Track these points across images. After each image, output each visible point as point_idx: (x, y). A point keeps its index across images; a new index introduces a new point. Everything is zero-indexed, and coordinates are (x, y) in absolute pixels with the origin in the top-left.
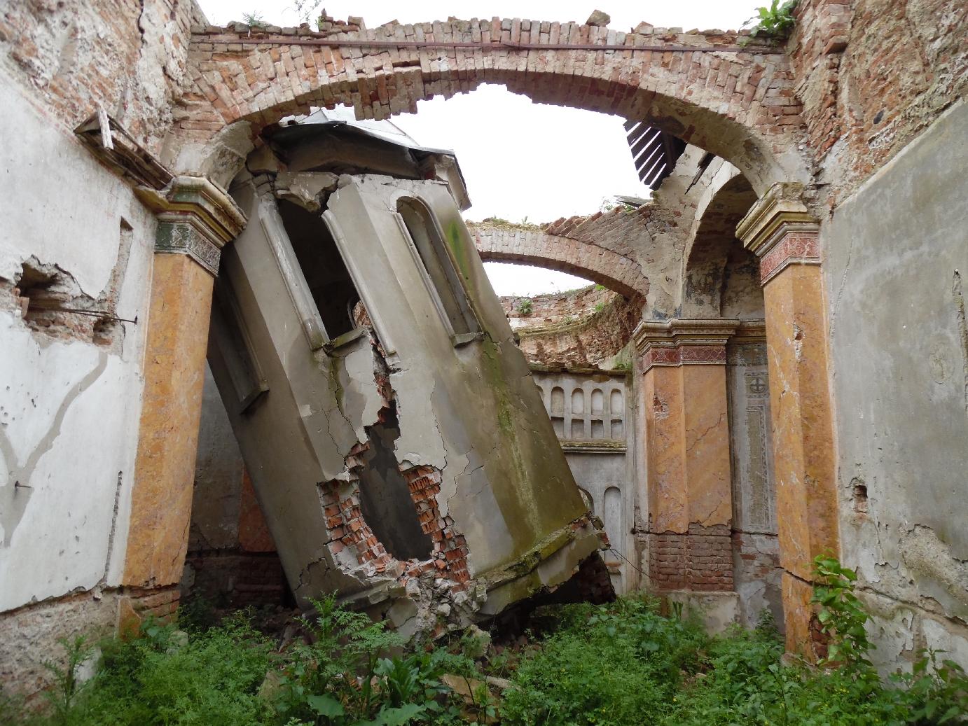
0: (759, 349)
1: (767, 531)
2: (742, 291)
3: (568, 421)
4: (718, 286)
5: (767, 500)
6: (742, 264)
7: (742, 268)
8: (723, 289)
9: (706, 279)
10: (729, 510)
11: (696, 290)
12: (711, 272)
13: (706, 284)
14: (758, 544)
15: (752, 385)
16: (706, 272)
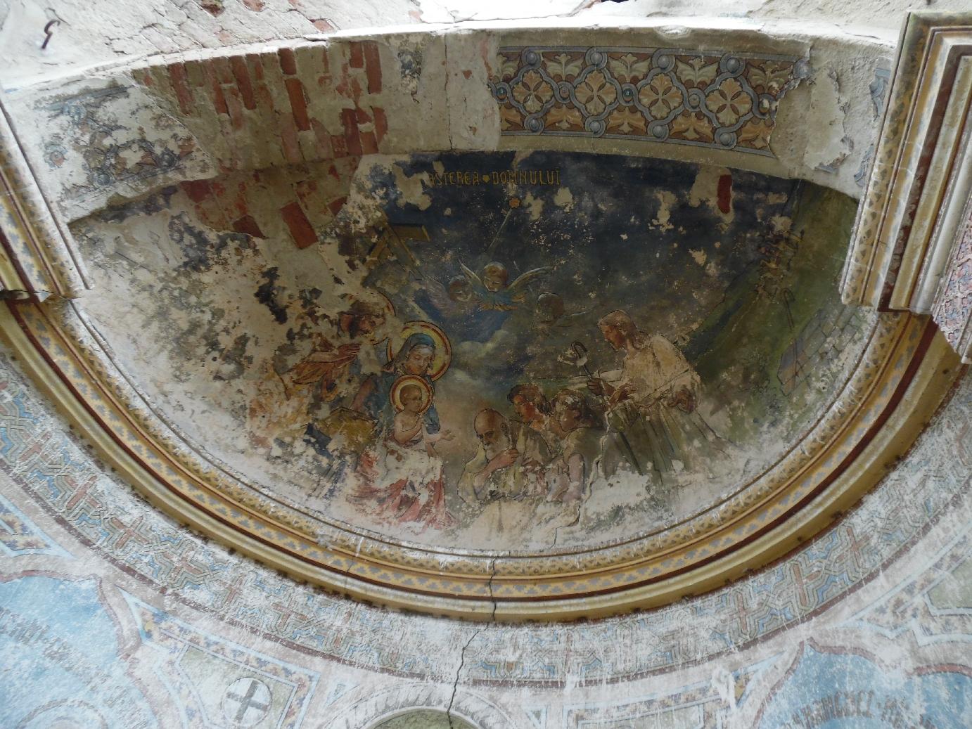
0: (16, 402)
2: (133, 264)
3: (604, 682)
4: (125, 190)
6: (199, 227)
7: (190, 230)
8: (117, 211)
9: (127, 146)
11: (81, 124)
12: (158, 150)
13: (115, 150)
16: (151, 136)
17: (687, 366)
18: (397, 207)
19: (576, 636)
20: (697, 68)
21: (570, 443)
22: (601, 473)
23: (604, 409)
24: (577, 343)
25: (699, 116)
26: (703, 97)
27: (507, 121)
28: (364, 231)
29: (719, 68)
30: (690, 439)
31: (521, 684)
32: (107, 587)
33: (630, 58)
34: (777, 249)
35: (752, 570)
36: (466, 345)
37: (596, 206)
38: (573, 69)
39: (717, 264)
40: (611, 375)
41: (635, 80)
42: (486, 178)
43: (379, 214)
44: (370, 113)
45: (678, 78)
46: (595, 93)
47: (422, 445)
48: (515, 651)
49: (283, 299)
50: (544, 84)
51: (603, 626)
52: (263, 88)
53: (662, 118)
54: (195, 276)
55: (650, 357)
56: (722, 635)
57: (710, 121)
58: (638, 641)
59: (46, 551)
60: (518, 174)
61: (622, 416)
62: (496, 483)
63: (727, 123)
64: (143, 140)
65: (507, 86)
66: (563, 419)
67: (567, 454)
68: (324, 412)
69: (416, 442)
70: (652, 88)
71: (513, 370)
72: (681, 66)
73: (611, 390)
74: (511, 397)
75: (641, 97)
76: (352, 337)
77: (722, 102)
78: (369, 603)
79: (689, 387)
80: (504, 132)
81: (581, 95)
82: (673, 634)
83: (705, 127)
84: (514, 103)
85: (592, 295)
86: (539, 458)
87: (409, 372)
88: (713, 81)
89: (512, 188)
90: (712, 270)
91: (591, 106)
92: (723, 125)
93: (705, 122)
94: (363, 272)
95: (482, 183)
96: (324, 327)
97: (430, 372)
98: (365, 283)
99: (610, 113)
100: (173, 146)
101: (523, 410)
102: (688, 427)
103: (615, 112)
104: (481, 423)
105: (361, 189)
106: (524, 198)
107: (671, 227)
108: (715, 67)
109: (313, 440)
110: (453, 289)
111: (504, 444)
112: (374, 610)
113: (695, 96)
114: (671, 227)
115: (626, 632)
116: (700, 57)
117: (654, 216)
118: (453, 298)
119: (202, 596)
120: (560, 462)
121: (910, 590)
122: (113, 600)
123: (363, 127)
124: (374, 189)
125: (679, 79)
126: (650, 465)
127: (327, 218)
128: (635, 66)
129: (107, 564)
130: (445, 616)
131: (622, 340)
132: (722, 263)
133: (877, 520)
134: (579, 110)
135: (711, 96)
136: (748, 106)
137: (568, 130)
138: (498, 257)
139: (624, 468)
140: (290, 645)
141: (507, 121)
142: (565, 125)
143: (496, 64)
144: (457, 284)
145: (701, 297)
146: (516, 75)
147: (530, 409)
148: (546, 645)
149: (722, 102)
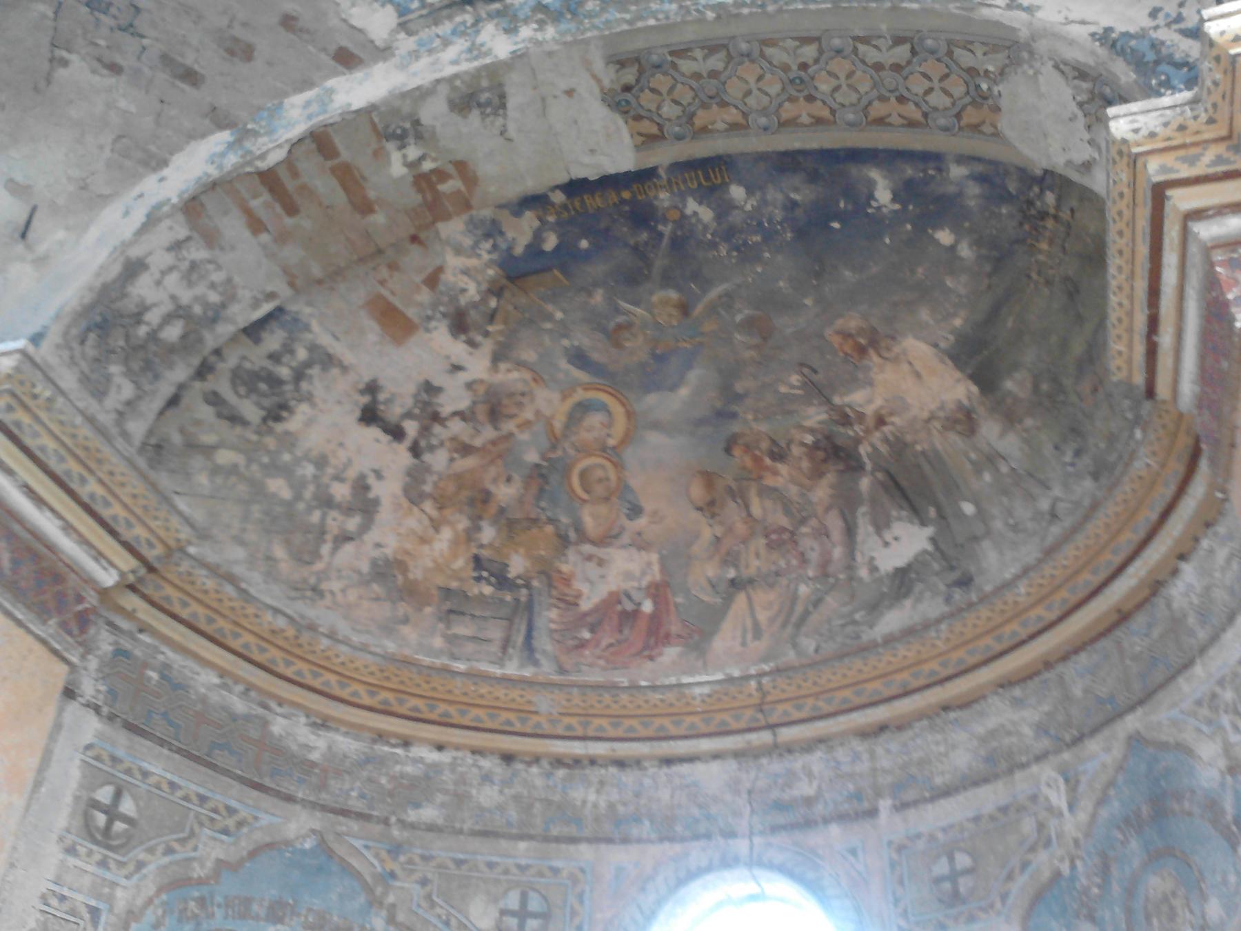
12: (197, 310)
15: (95, 805)
16: (186, 296)
17: (958, 375)
18: (515, 258)
19: (880, 751)
20: (884, 49)
21: (822, 492)
22: (871, 529)
23: (857, 441)
24: (802, 365)
25: (902, 100)
26: (901, 80)
27: (640, 134)
28: (477, 298)
29: (913, 48)
30: (978, 471)
31: (826, 821)
32: (330, 838)
33: (791, 44)
34: (1045, 228)
35: (1067, 654)
36: (652, 399)
37: (788, 198)
38: (716, 62)
39: (970, 246)
40: (856, 397)
41: (804, 66)
42: (626, 195)
43: (491, 272)
44: (451, 169)
45: (863, 62)
46: (753, 85)
47: (626, 538)
48: (810, 782)
49: (394, 412)
50: (679, 86)
51: (910, 733)
52: (303, 188)
53: (852, 105)
54: (279, 427)
55: (905, 367)
56: (1046, 732)
57: (917, 105)
58: (954, 747)
59: (257, 825)
60: (669, 181)
61: (883, 449)
62: (736, 567)
63: (941, 107)
64: (179, 307)
65: (628, 96)
66: (805, 464)
67: (820, 510)
68: (488, 533)
69: (616, 537)
70: (829, 73)
71: (724, 415)
72: (862, 48)
73: (861, 417)
74: (728, 450)
75: (817, 84)
76: (496, 428)
77: (927, 84)
78: (621, 763)
79: (965, 402)
80: (638, 148)
81: (734, 90)
82: (993, 734)
83: (911, 111)
84: (643, 113)
85: (808, 302)
86: (784, 522)
87: (584, 450)
88: (909, 63)
89: (664, 198)
90: (966, 251)
91: (751, 101)
92: (935, 109)
93: (911, 106)
94: (488, 346)
95: (623, 202)
96: (456, 427)
97: (611, 442)
98: (497, 358)
99: (780, 105)
100: (214, 298)
101: (748, 462)
102: (973, 456)
103: (787, 104)
104: (697, 491)
105: (459, 251)
106: (685, 206)
107: (897, 207)
108: (907, 47)
109: (485, 574)
110: (615, 336)
111: (732, 511)
112: (628, 770)
113: (889, 78)
114: (897, 207)
115: (939, 737)
116: (885, 38)
117: (871, 196)
118: (618, 345)
119: (429, 813)
120: (813, 522)
121: (1221, 683)
122: (340, 850)
123: (446, 187)
124: (476, 245)
125: (863, 62)
126: (932, 512)
127: (425, 296)
128: (799, 51)
129: (318, 814)
130: (717, 756)
131: (862, 351)
132: (978, 243)
133: (1192, 595)
134: (737, 108)
135: (911, 77)
136: (963, 89)
137: (726, 130)
138: (667, 280)
139: (899, 519)
140: (547, 839)
141: (640, 134)
142: (720, 126)
143: (609, 77)
144: (620, 327)
145: (957, 284)
146: (638, 81)
147: (757, 460)
148: (846, 768)
149: (927, 84)
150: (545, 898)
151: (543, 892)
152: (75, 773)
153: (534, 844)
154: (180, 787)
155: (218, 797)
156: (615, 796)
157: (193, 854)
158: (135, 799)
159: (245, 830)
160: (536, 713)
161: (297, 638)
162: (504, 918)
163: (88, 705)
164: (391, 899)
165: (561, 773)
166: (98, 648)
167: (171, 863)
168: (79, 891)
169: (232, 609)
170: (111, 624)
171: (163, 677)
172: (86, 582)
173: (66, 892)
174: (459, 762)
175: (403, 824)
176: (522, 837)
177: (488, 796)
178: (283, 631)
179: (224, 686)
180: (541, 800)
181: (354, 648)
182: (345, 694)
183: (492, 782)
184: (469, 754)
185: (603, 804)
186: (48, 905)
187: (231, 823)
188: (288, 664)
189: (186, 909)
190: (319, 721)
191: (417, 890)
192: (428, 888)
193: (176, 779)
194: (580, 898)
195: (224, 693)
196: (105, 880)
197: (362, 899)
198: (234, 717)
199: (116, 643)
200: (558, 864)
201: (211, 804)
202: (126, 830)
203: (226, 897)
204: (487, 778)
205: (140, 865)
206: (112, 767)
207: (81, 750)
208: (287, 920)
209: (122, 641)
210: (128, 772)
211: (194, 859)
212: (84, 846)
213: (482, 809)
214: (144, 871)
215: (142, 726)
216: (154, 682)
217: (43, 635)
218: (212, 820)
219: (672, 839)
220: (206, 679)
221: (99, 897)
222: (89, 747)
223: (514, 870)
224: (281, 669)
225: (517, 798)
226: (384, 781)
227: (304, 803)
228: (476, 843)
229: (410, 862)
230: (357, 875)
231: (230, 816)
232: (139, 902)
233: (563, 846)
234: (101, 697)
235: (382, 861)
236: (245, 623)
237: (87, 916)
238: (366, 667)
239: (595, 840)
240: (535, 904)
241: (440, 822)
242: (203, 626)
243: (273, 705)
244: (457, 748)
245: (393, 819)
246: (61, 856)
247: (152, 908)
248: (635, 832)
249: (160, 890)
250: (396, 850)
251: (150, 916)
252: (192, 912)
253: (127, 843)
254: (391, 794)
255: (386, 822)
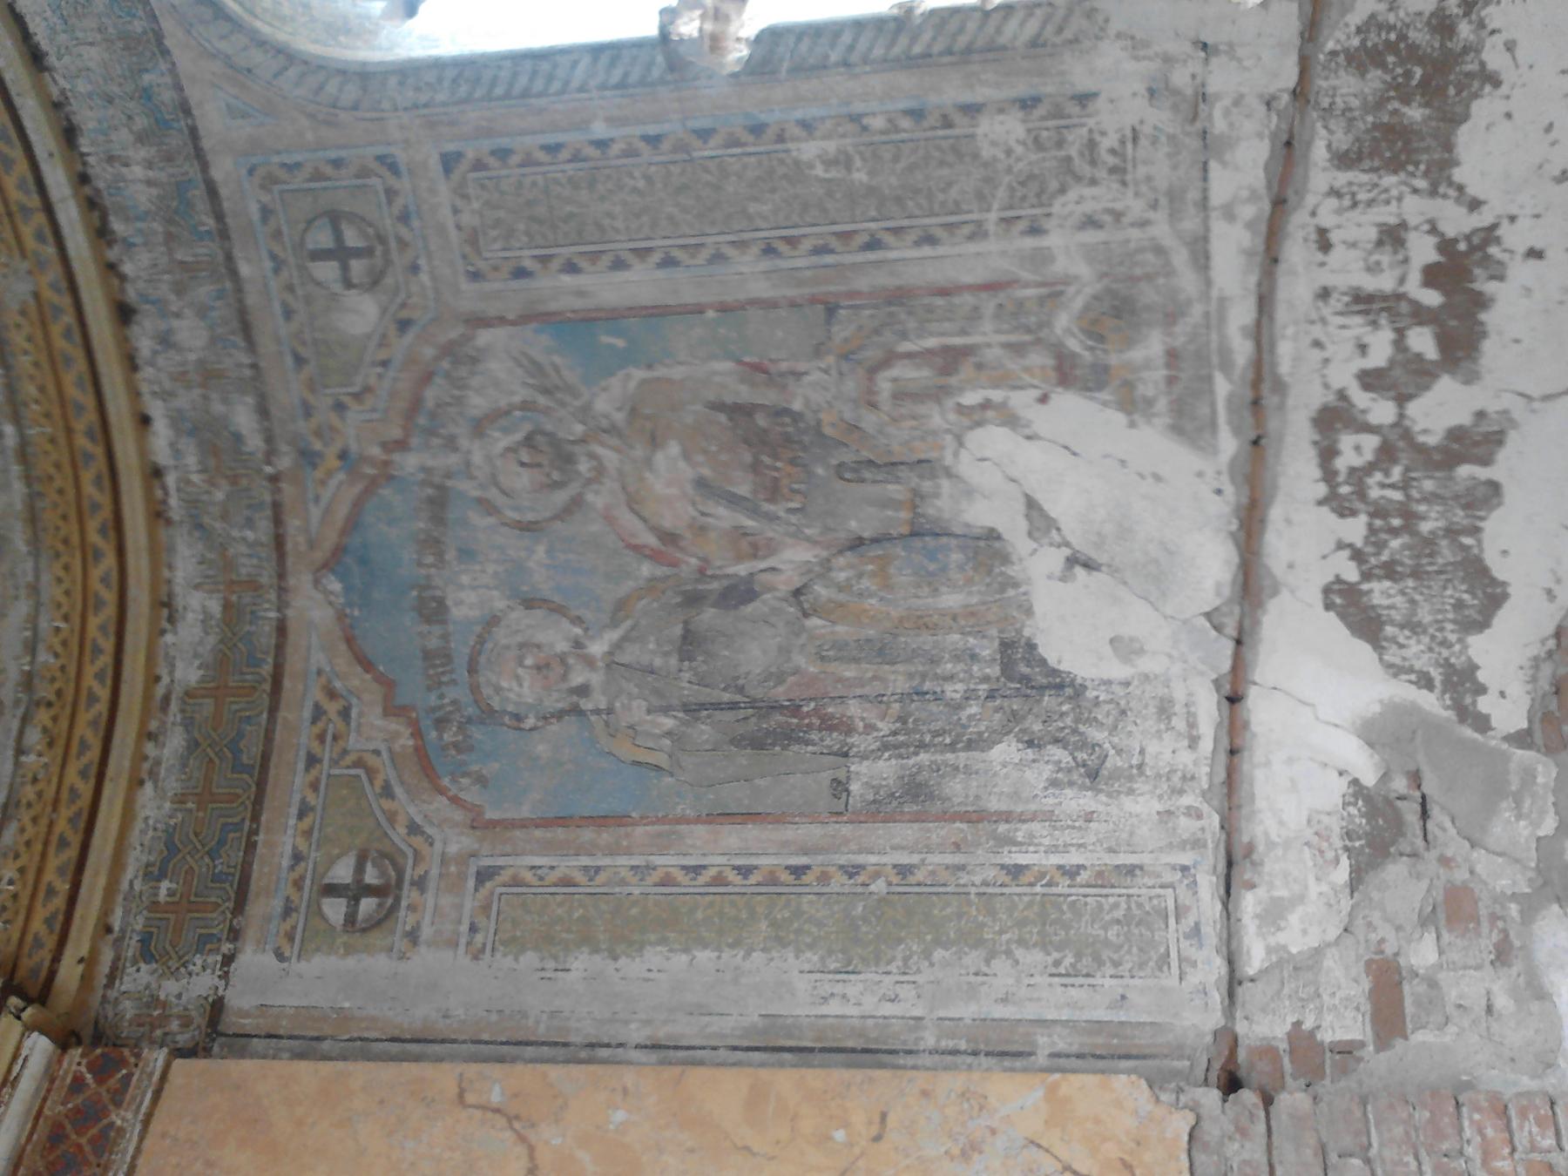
1: (1208, 885)
5: (1016, 871)
10: (1081, 1087)
14: (1297, 937)
15: (350, 919)
32: (319, 556)
78: (69, 134)
112: (76, 119)
119: (244, 418)
140: (224, 234)
150: (310, 222)
151: (302, 226)
152: (320, 963)
153: (238, 253)
154: (303, 801)
155: (304, 739)
156: (124, 135)
157: (385, 755)
158: (332, 861)
159: (338, 684)
160: (36, 296)
161: (49, 704)
162: (355, 281)
163: (225, 976)
164: (375, 451)
165: (117, 226)
166: (147, 987)
167: (402, 783)
168: (460, 907)
169: (35, 820)
170: (112, 977)
171: (162, 875)
172: (52, 1081)
173: (465, 928)
174: (156, 388)
175: (270, 455)
176: (234, 273)
177: (191, 334)
178: (45, 730)
179: (153, 774)
180: (170, 252)
181: (38, 606)
182: (110, 596)
183: (170, 331)
184: (140, 375)
185: (143, 153)
186: (484, 945)
187: (332, 708)
188: (93, 699)
189: (455, 745)
190: (165, 612)
191: (355, 414)
192: (346, 399)
193: (294, 810)
194: (292, 168)
195: (163, 773)
196: (441, 875)
197: (386, 492)
198: (193, 745)
199: (135, 962)
200: (254, 210)
201: (316, 747)
202: (374, 865)
203: (429, 689)
204: (166, 340)
205: (414, 829)
206: (296, 910)
207: (285, 965)
208: (438, 593)
209: (130, 954)
210: (298, 884)
211: (390, 750)
212: (406, 920)
213: (213, 340)
214: (418, 819)
215: (235, 886)
216: (174, 886)
217: (138, 1127)
218: (335, 738)
219: (159, 37)
220: (153, 806)
221: (462, 877)
222: (280, 956)
223: (285, 274)
224: (102, 707)
225: (180, 290)
226: (219, 495)
227: (281, 606)
228: (266, 344)
229: (318, 434)
230: (358, 505)
231: (325, 713)
232: (458, 815)
233: (226, 205)
234: (210, 959)
235: (330, 473)
236: (50, 793)
237: (488, 885)
238: (59, 580)
239: (200, 155)
240: (322, 238)
241: (250, 400)
242: (72, 853)
243: (160, 690)
244: (135, 394)
245: (269, 469)
246: (423, 949)
247: (462, 795)
248: (168, 96)
249: (442, 791)
250: (308, 457)
251: (472, 795)
252: (455, 735)
253: (390, 857)
254: (234, 480)
255: (274, 479)
